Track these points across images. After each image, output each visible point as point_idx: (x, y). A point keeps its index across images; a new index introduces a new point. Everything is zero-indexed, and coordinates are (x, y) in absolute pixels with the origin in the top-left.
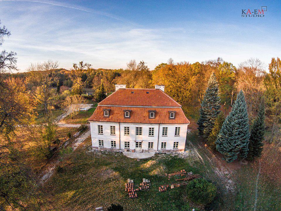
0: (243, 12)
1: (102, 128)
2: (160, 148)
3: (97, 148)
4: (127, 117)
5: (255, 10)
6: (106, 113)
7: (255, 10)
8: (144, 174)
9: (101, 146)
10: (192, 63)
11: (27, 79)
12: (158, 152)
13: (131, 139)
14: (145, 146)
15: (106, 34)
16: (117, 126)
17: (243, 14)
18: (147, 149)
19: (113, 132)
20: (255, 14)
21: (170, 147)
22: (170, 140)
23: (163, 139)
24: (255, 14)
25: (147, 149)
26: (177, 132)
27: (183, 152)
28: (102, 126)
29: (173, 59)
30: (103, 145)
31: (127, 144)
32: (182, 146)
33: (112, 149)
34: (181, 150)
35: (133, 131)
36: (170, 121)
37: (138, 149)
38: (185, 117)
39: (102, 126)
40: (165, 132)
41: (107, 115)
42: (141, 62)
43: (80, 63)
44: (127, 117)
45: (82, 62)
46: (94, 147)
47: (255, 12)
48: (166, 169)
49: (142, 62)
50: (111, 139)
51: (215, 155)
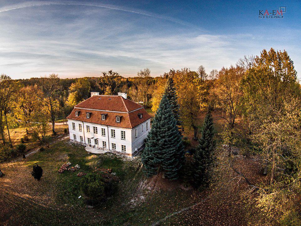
0: (260, 13)
1: (124, 134)
2: (111, 148)
3: (73, 140)
4: (118, 121)
5: (273, 11)
6: (117, 119)
7: (273, 11)
8: (82, 164)
9: (114, 149)
10: (14, 79)
11: (73, 85)
12: (109, 151)
13: (88, 135)
14: (100, 145)
15: (172, 40)
16: (106, 128)
17: (260, 15)
18: (102, 147)
19: (123, 137)
20: (273, 15)
21: (119, 149)
22: (118, 142)
23: (112, 141)
24: (273, 15)
25: (102, 147)
26: (123, 134)
27: (131, 156)
28: (124, 132)
29: (204, 66)
30: (115, 148)
31: (89, 140)
32: (129, 151)
33: (81, 143)
34: (128, 154)
35: (92, 130)
36: (116, 125)
37: (96, 146)
38: (130, 123)
39: (124, 132)
40: (113, 135)
41: (119, 121)
42: (171, 71)
43: (109, 72)
44: (118, 121)
45: (111, 71)
46: (71, 140)
47: (273, 13)
48: (99, 164)
49: (172, 70)
50: (102, 140)
51: (4, 127)
